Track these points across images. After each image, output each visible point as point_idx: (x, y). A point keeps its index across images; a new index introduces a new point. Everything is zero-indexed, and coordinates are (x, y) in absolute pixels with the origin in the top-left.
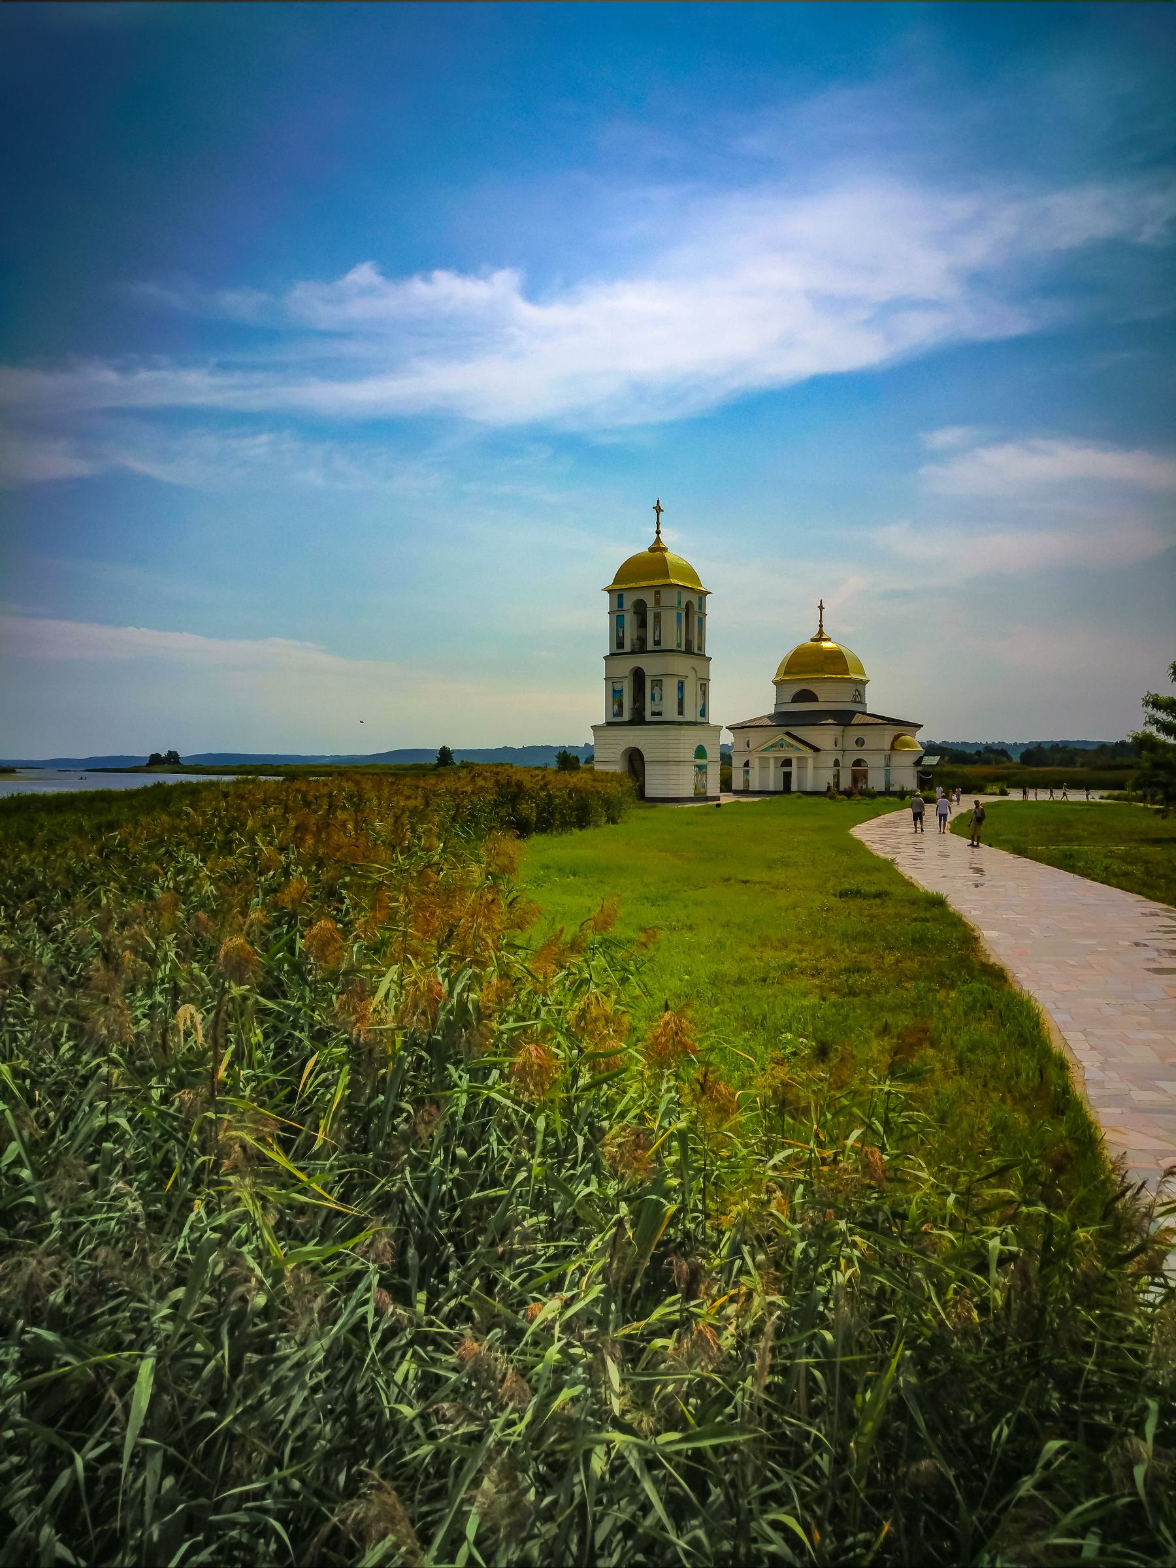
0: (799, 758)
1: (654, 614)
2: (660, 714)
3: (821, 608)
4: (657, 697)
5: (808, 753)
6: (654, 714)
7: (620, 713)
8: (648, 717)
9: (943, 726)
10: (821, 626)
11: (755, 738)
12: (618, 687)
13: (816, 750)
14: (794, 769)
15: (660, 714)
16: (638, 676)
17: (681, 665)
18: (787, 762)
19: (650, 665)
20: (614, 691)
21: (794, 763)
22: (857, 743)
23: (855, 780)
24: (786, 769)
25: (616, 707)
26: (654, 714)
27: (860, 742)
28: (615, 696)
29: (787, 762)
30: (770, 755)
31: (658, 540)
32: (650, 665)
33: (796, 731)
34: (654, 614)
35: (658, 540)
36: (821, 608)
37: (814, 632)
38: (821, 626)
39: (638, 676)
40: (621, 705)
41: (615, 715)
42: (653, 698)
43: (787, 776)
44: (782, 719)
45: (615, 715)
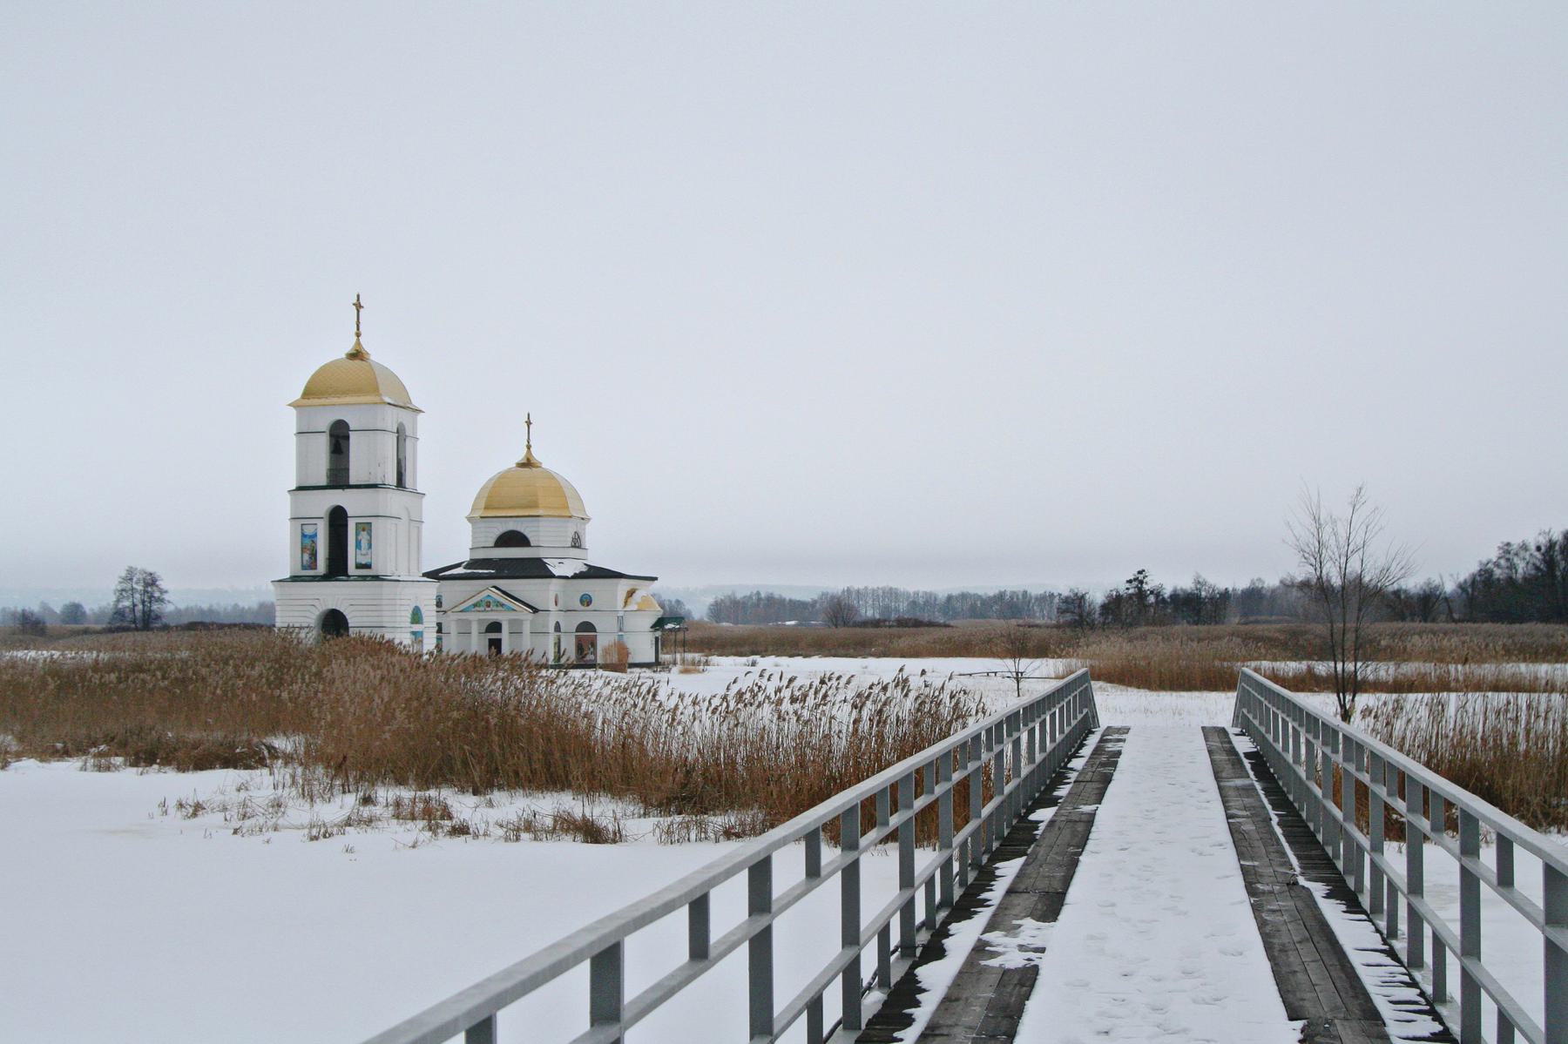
0: (511, 622)
1: (346, 438)
2: (368, 566)
3: (358, 306)
4: (364, 544)
5: (526, 615)
6: (359, 566)
7: (313, 564)
8: (352, 569)
9: (696, 590)
10: (529, 447)
11: (456, 592)
12: (309, 530)
13: (535, 610)
14: (505, 636)
15: (368, 566)
16: (338, 518)
17: (392, 501)
18: (495, 627)
19: (351, 501)
20: (304, 536)
21: (505, 628)
22: (582, 602)
23: (580, 649)
24: (494, 636)
25: (306, 557)
26: (359, 566)
27: (586, 600)
28: (307, 545)
29: (495, 627)
30: (473, 617)
31: (358, 343)
32: (351, 501)
33: (504, 584)
34: (346, 438)
35: (358, 343)
36: (358, 306)
37: (521, 456)
38: (529, 447)
39: (338, 518)
40: (314, 555)
41: (304, 568)
42: (358, 545)
43: (496, 644)
44: (479, 568)
45: (304, 568)
